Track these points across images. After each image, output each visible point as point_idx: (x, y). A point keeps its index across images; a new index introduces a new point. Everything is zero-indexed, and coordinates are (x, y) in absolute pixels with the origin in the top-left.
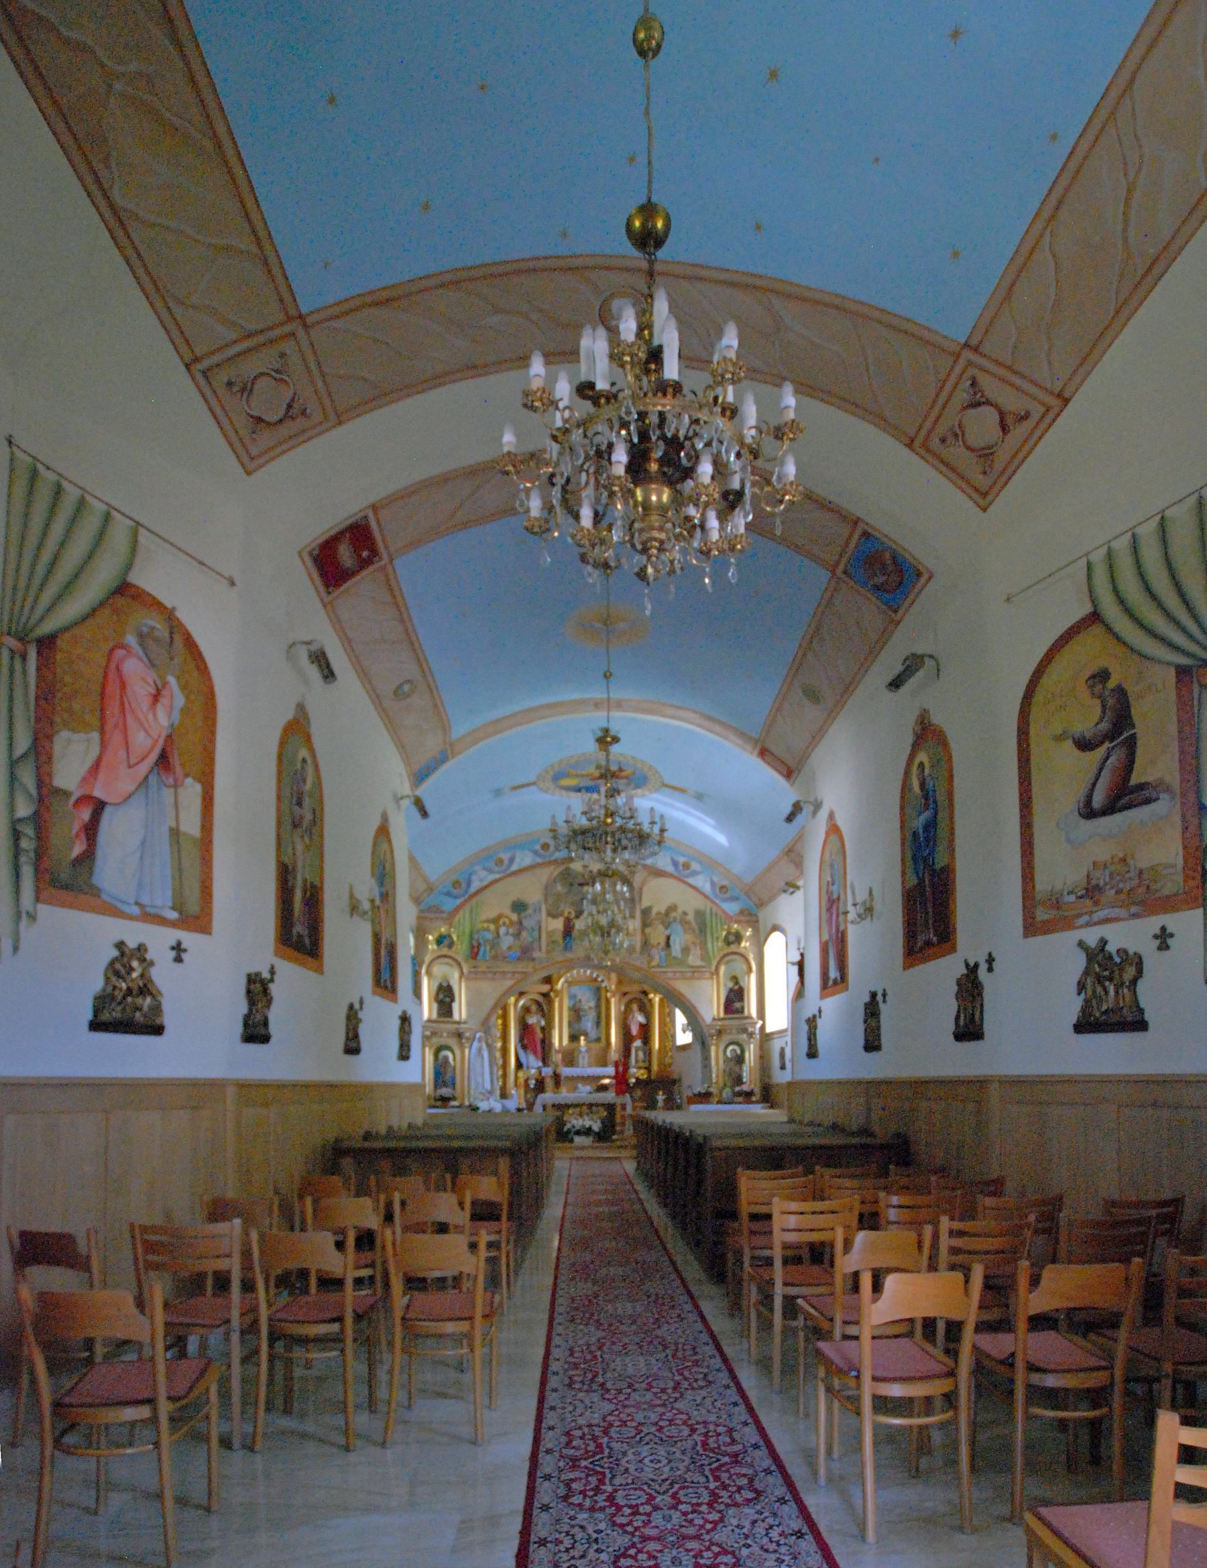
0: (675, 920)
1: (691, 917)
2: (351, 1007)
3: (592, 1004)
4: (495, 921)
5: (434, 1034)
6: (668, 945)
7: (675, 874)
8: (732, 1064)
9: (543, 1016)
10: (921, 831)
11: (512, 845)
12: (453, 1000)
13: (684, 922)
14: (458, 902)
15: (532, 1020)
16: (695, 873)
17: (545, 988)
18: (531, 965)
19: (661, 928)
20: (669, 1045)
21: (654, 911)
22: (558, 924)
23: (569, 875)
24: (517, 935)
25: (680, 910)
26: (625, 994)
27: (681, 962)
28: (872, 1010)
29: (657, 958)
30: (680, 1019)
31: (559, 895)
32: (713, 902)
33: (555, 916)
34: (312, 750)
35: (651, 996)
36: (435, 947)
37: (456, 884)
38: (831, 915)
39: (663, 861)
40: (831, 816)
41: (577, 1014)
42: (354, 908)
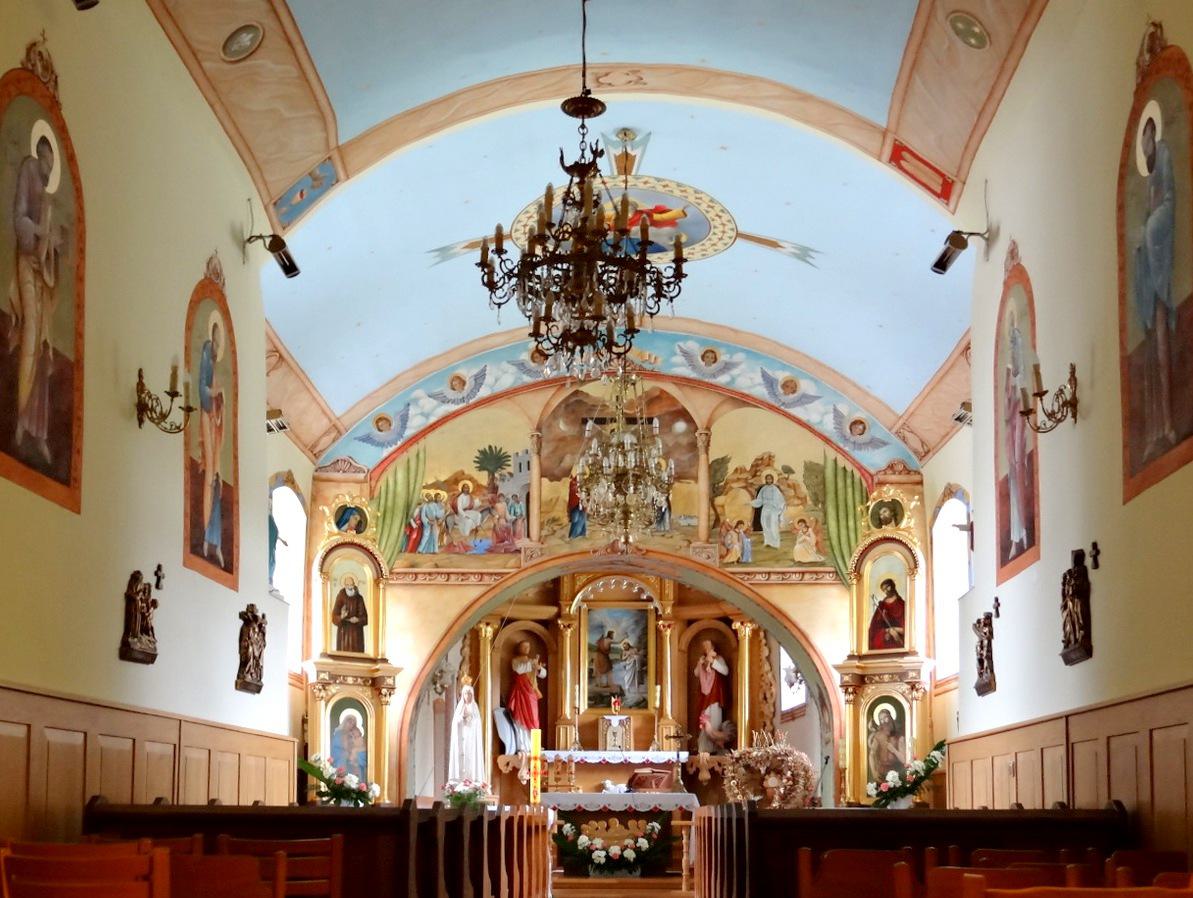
0: (769, 479)
1: (798, 477)
2: (136, 577)
4: (451, 484)
5: (334, 678)
6: (757, 525)
7: (772, 401)
8: (882, 737)
9: (544, 660)
10: (1149, 245)
15: (523, 668)
16: (806, 399)
17: (549, 612)
18: (512, 561)
19: (744, 496)
20: (768, 710)
21: (731, 467)
22: (563, 489)
23: (580, 402)
24: (488, 510)
25: (778, 465)
26: (690, 622)
27: (776, 555)
28: (1077, 585)
29: (737, 547)
30: (786, 662)
31: (562, 439)
32: (839, 449)
33: (554, 478)
34: (61, 130)
35: (736, 625)
36: (335, 529)
37: (382, 421)
38: (1014, 428)
39: (748, 379)
40: (1013, 253)
41: (604, 657)
42: (143, 409)
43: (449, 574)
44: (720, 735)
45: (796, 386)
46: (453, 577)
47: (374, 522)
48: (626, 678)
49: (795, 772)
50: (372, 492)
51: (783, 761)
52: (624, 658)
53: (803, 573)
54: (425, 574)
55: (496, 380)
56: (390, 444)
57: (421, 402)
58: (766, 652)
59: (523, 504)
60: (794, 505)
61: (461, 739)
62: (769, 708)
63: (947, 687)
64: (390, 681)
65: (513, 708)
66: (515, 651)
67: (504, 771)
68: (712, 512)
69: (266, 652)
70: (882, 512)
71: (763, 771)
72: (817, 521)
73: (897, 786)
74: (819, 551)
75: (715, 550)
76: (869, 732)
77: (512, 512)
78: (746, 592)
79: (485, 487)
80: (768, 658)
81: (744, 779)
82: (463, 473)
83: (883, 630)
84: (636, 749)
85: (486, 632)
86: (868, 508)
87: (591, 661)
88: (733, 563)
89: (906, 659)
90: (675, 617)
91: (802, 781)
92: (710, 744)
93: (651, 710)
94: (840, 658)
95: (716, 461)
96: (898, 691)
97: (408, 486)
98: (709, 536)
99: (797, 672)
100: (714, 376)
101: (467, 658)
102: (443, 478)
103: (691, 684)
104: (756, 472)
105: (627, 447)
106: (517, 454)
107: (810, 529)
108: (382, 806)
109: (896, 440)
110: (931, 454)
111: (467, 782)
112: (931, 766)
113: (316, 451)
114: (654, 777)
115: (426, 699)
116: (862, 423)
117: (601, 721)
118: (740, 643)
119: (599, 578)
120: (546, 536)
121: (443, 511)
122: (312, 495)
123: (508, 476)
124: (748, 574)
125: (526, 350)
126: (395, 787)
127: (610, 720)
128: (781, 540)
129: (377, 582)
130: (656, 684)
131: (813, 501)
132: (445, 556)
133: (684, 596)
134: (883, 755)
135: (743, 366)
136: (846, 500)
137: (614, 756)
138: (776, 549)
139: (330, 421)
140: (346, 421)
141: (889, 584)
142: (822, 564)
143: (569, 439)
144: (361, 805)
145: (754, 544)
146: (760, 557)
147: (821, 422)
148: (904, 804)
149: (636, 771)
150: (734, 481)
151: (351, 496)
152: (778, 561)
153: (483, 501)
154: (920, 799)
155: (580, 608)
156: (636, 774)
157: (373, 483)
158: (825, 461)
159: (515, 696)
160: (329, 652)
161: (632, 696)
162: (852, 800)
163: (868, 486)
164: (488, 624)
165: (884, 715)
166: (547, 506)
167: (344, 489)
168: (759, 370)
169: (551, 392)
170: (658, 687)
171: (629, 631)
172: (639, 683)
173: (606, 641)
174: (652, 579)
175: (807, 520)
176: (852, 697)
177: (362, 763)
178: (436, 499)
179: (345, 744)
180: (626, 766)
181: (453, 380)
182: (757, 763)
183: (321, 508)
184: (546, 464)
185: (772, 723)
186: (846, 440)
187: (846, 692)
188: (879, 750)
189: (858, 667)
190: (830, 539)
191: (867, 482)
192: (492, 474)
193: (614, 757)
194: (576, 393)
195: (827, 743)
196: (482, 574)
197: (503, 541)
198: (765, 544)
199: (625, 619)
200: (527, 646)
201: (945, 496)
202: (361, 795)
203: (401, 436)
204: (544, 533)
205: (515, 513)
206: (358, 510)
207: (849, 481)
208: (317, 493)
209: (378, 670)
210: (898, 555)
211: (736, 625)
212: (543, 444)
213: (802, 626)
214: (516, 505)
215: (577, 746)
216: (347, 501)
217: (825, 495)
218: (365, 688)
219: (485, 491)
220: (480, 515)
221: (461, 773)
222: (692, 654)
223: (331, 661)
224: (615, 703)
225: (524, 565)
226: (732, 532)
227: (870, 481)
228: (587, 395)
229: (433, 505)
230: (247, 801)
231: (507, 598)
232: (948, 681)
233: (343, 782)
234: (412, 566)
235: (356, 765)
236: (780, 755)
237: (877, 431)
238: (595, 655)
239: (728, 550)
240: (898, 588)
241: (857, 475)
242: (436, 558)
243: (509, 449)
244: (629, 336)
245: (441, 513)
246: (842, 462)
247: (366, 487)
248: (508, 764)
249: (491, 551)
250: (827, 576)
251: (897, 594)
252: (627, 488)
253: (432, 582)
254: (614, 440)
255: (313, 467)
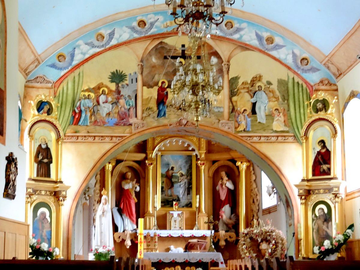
0: (260, 87)
3: (184, 172)
5: (35, 191)
6: (254, 112)
7: (261, 48)
8: (320, 222)
9: (138, 182)
11: (113, 21)
12: (51, 162)
13: (268, 91)
14: (63, 73)
15: (128, 186)
16: (278, 47)
17: (141, 156)
18: (128, 129)
19: (247, 96)
20: (255, 208)
21: (240, 81)
22: (154, 93)
23: (163, 48)
24: (115, 103)
25: (264, 80)
26: (214, 162)
29: (243, 123)
30: (266, 182)
31: (154, 67)
32: (295, 73)
33: (150, 86)
35: (238, 164)
36: (36, 113)
37: (60, 57)
39: (248, 36)
41: (169, 180)
43: (95, 137)
44: (230, 222)
45: (273, 41)
46: (97, 138)
47: (56, 109)
48: (181, 192)
49: (277, 241)
50: (55, 93)
51: (270, 235)
52: (180, 181)
53: (278, 137)
54: (82, 136)
55: (120, 36)
56: (65, 68)
57: (81, 47)
58: (253, 177)
59: (133, 100)
60: (272, 101)
61: (101, 224)
62: (256, 207)
63: (353, 196)
64: (64, 193)
65: (122, 207)
66: (123, 177)
67: (117, 241)
68: (231, 105)
69: (18, 177)
70: (318, 105)
71: (259, 240)
72: (284, 110)
73: (330, 248)
74: (285, 125)
75: (232, 124)
76: (313, 220)
77: (128, 104)
78: (249, 146)
79: (114, 91)
80: (255, 181)
81: (249, 245)
82: (103, 84)
83: (320, 166)
84: (186, 229)
85: (108, 167)
86: (310, 103)
87: (163, 183)
88: (242, 131)
89: (332, 181)
90: (206, 159)
91: (280, 246)
92: (225, 226)
93: (194, 208)
94: (298, 181)
95: (233, 78)
96: (328, 198)
97: (74, 90)
98: (229, 117)
99: (273, 188)
100: (231, 35)
101: (98, 181)
102: (92, 87)
103: (215, 195)
104: (253, 84)
105: (198, 71)
106: (131, 74)
107: (281, 114)
108: (59, 259)
109: (324, 68)
110: (342, 76)
111: (104, 247)
112: (347, 238)
113: (27, 72)
114: (198, 244)
115: (80, 202)
116: (306, 59)
117: (168, 215)
118: (241, 174)
119: (166, 139)
120: (145, 117)
121: (92, 104)
122: (24, 95)
123: (126, 86)
124: (250, 137)
125: (136, 20)
126: (65, 250)
127: (173, 214)
128: (266, 119)
129: (58, 140)
130: (197, 195)
131: (282, 99)
132: (93, 127)
133: (211, 148)
134: (320, 232)
135: (246, 30)
136: (299, 98)
137: (175, 233)
138: (264, 124)
139: (35, 56)
140: (43, 56)
141: (322, 142)
142: (287, 132)
143: (157, 66)
144: (49, 259)
145: (252, 121)
146: (255, 128)
147: (286, 59)
148: (333, 258)
149: (190, 241)
150: (241, 89)
151: (45, 95)
152: (264, 130)
153: (113, 99)
154: (341, 255)
155: (157, 154)
156: (189, 243)
157: (56, 89)
158: (288, 79)
159: (123, 201)
160: (32, 178)
161: (184, 200)
162: (305, 256)
163: (310, 92)
164: (109, 163)
165: (321, 211)
166: (146, 101)
167: (41, 91)
168: (255, 32)
169: (148, 42)
170: (198, 196)
171: (182, 167)
172: (188, 194)
173: (171, 172)
174: (195, 139)
175: (279, 109)
176: (304, 201)
177: (49, 237)
178: (89, 97)
179: (40, 228)
180: (181, 238)
181: (98, 36)
182: (256, 236)
183: (29, 102)
184: (145, 79)
185: (257, 215)
186: (298, 68)
187: (301, 199)
188: (318, 230)
189: (307, 186)
190: (291, 119)
191: (309, 89)
192: (117, 84)
193: (175, 234)
194: (161, 43)
195: (290, 225)
196: (112, 137)
197: (123, 119)
198: (258, 121)
199: (180, 160)
200: (129, 175)
201: (350, 97)
202: (49, 254)
203: (70, 64)
204: (144, 115)
205: (129, 105)
206: (48, 103)
207: (300, 89)
208: (27, 94)
209: (58, 187)
210: (327, 127)
211: (238, 164)
212: (144, 69)
213: (278, 164)
214: (130, 101)
215: (156, 228)
216: (43, 98)
217: (288, 96)
218: (51, 197)
219: (114, 94)
220: (111, 106)
221: (101, 242)
222: (215, 179)
223: (33, 182)
224: (175, 204)
225: (134, 132)
226: (241, 115)
227: (311, 89)
228: (166, 44)
229: (87, 101)
230: (10, 258)
231: (123, 150)
232: (353, 193)
233: (40, 247)
234: (76, 132)
235: (46, 238)
236: (268, 232)
237: (314, 63)
238: (165, 179)
239: (239, 125)
240: (327, 145)
241: (305, 86)
242: (88, 128)
243: (126, 72)
244: (222, 15)
245: (91, 105)
246: (297, 79)
247: (52, 91)
248: (119, 237)
249: (117, 124)
250: (290, 138)
251: (326, 148)
252: (198, 92)
253: (86, 141)
254: (191, 68)
255: (25, 81)
